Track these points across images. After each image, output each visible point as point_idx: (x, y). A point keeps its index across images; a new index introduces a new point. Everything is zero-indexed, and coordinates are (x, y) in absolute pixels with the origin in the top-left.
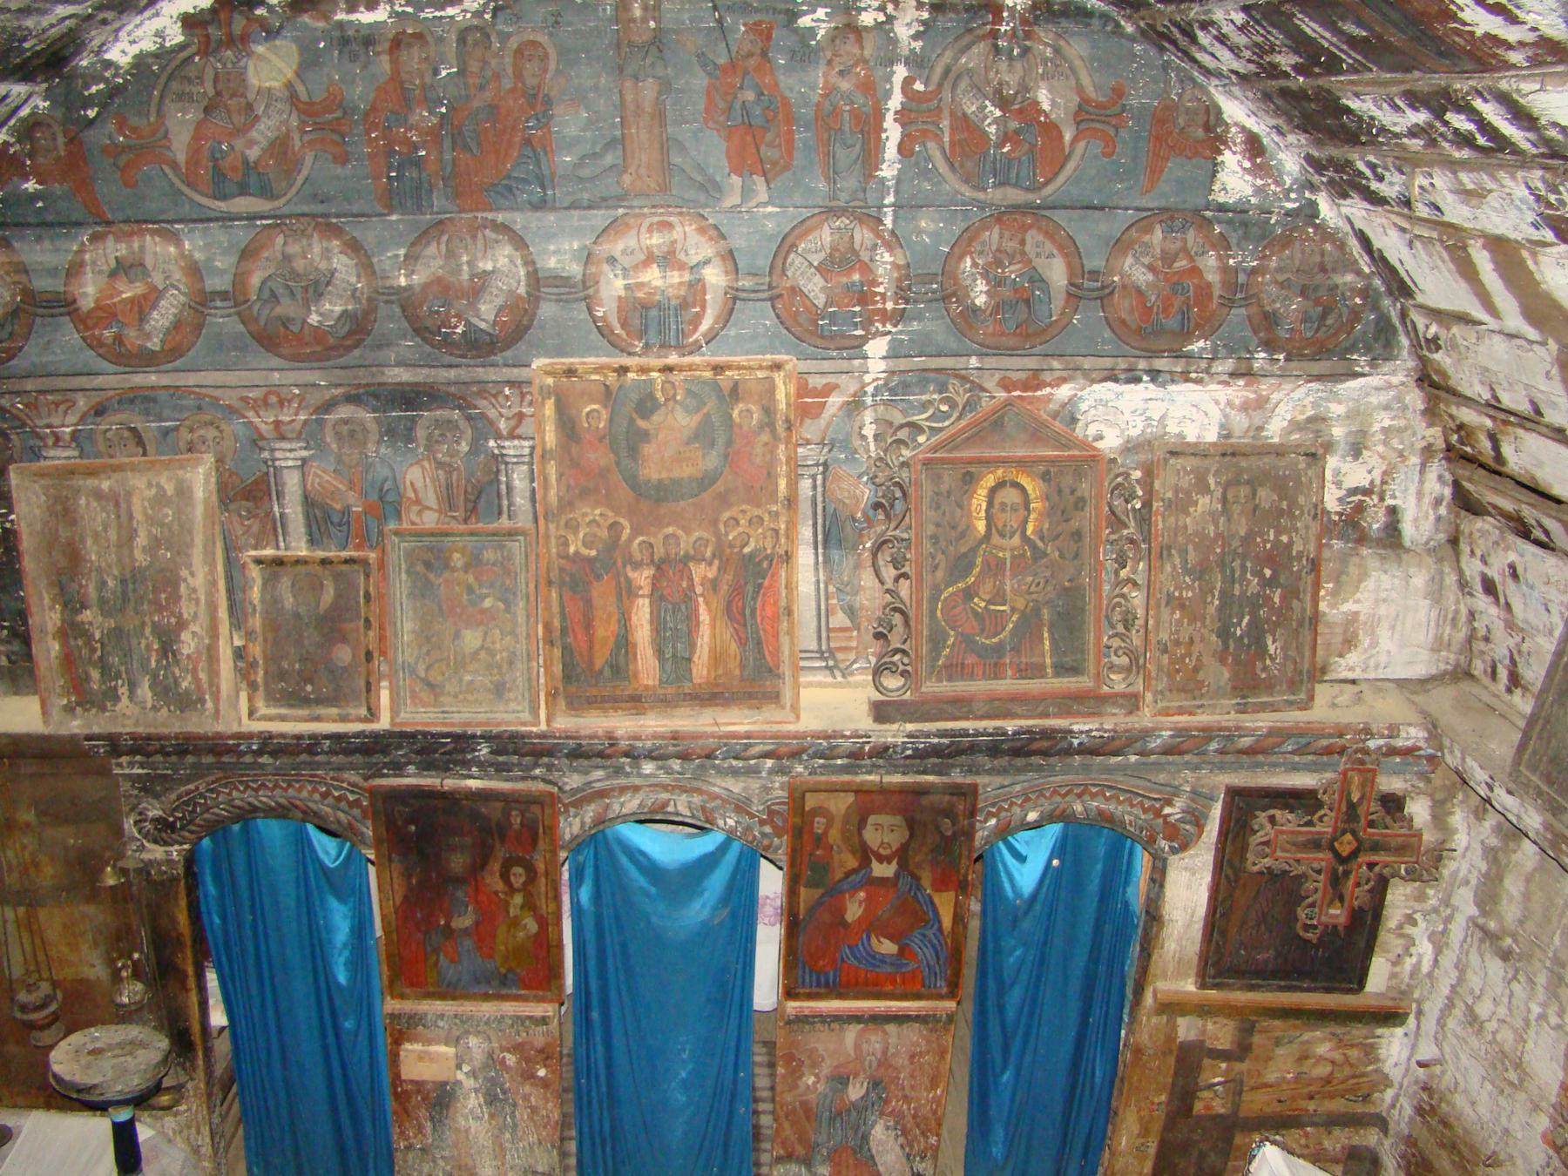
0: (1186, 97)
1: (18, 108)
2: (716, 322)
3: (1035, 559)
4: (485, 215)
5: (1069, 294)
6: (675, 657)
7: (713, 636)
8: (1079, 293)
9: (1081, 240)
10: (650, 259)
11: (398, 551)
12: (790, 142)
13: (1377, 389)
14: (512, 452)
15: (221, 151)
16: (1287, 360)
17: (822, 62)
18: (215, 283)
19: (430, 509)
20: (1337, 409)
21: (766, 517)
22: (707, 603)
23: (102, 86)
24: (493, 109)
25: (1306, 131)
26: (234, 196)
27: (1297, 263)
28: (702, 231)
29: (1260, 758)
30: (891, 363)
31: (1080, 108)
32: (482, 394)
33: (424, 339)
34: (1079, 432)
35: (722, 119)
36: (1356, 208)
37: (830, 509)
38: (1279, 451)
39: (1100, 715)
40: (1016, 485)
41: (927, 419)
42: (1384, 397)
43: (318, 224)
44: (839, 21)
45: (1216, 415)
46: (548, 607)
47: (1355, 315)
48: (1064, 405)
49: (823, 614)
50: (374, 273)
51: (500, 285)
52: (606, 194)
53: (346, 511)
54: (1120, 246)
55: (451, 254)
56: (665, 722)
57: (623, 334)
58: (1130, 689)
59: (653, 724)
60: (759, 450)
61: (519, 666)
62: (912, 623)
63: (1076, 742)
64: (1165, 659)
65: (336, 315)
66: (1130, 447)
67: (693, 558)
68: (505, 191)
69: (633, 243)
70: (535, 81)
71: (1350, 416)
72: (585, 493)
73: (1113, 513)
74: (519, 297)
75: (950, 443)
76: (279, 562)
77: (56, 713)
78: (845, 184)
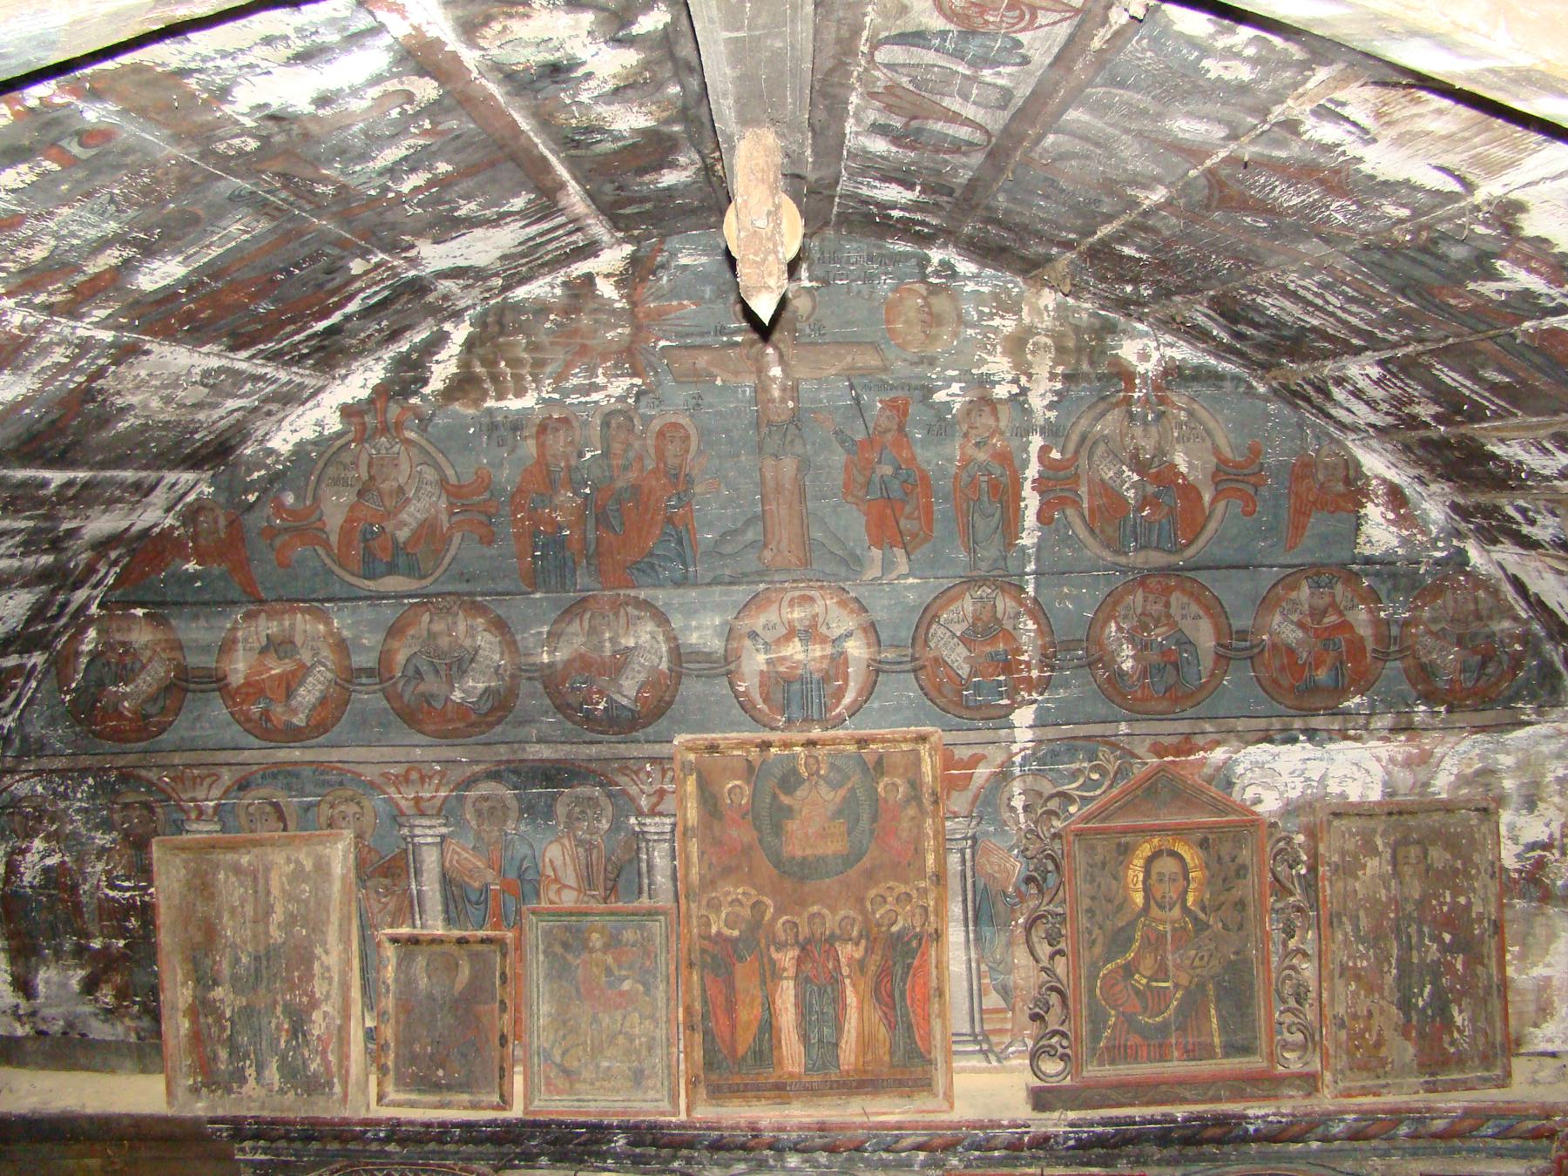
0: (1325, 451)
1: (185, 494)
2: (859, 694)
3: (1198, 932)
4: (628, 592)
6: (822, 1048)
7: (861, 1019)
10: (791, 633)
11: (535, 930)
12: (929, 512)
13: (1547, 737)
14: (653, 829)
15: (372, 532)
16: (1449, 711)
18: (360, 660)
20: (1506, 761)
21: (914, 894)
22: (854, 985)
25: (1449, 480)
26: (382, 576)
27: (1451, 612)
28: (842, 604)
29: (1457, 1142)
30: (1039, 731)
32: (624, 770)
33: (565, 715)
35: (861, 494)
36: (1507, 554)
37: (981, 883)
38: (1447, 808)
39: (1276, 1097)
40: (1173, 854)
41: (1077, 789)
42: (1554, 746)
45: (1378, 771)
46: (688, 991)
47: (1516, 662)
48: (1218, 769)
49: (975, 994)
50: (517, 650)
51: (643, 661)
52: (747, 570)
53: (485, 889)
54: (1266, 603)
55: (593, 631)
56: (812, 1111)
57: (765, 708)
58: (1307, 1069)
59: (799, 1114)
60: (905, 824)
61: (659, 1052)
62: (1071, 1003)
63: (1251, 1128)
64: (1343, 1035)
65: (479, 692)
66: (1291, 810)
67: (839, 938)
68: (645, 568)
69: (774, 618)
70: (677, 461)
71: (1521, 766)
72: (727, 872)
74: (662, 673)
75: (1103, 813)
76: (414, 941)
77: (181, 1093)
78: (986, 554)
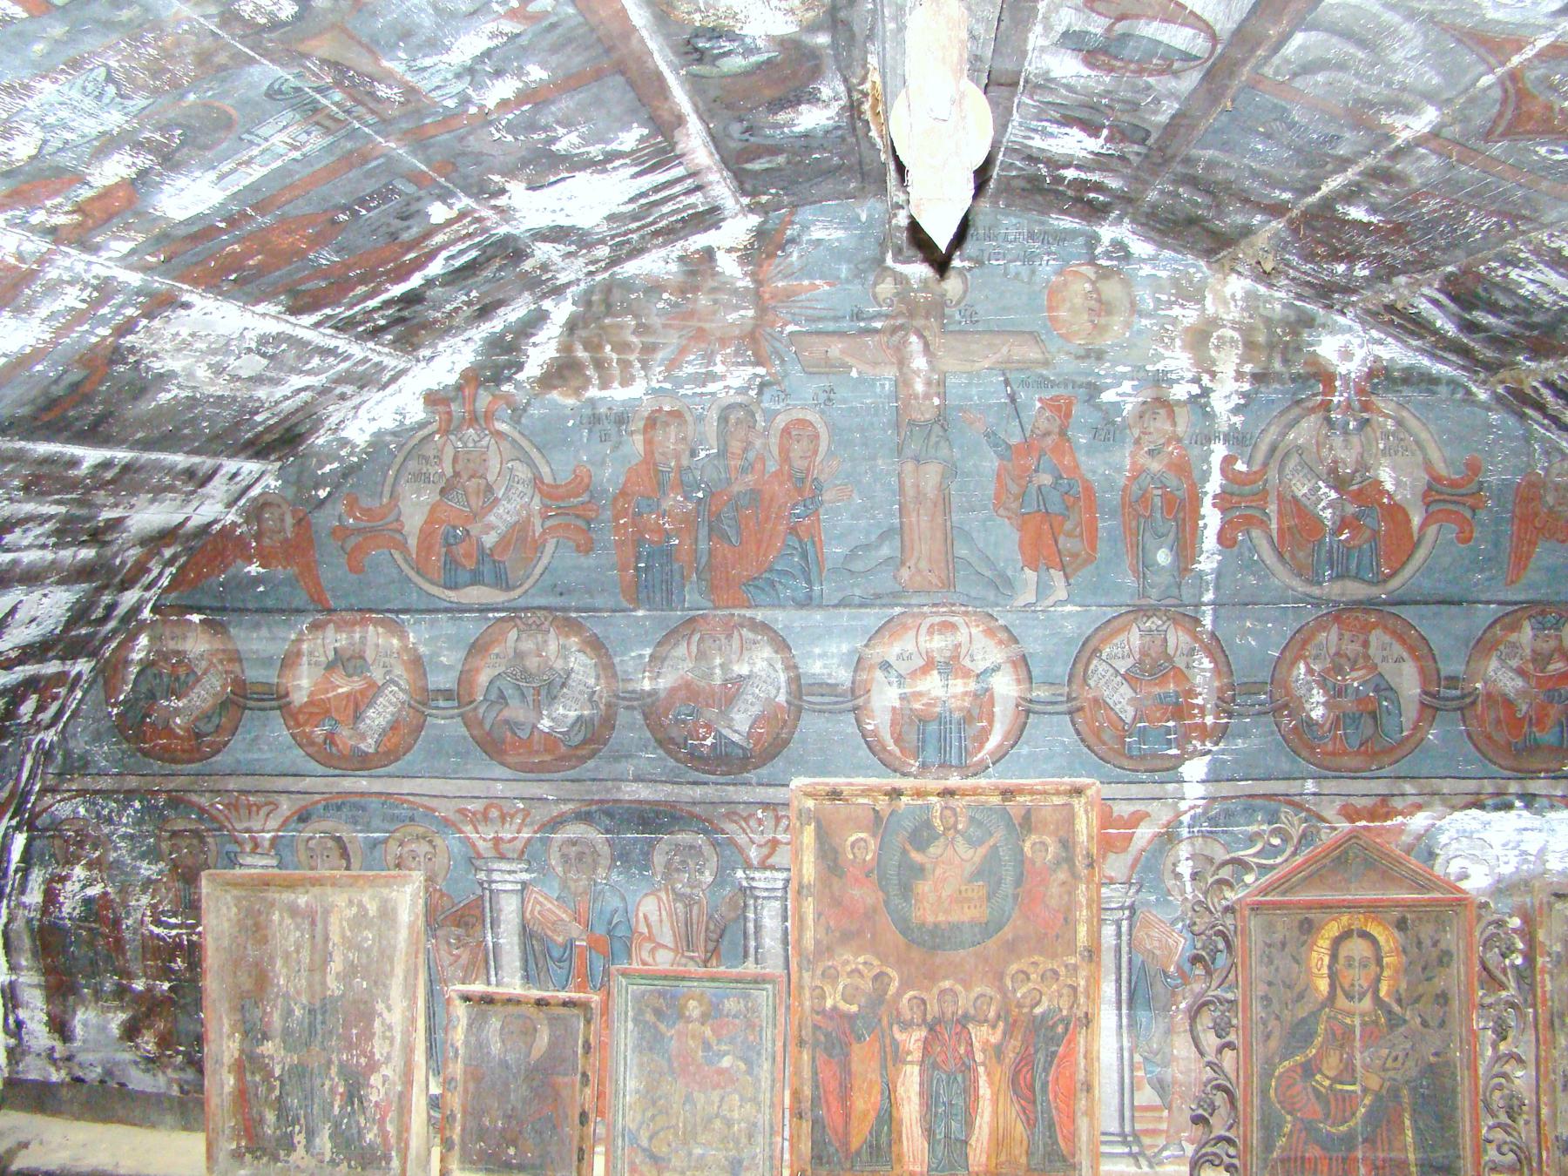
0: (1554, 471)
1: (249, 487)
2: (1006, 738)
5: (1422, 703)
7: (995, 1113)
8: (1435, 703)
9: (1436, 641)
10: (929, 665)
11: (625, 994)
14: (762, 885)
15: (455, 536)
17: (1129, 441)
18: (440, 680)
19: (665, 947)
21: (1062, 971)
23: (336, 465)
24: (755, 495)
28: (989, 632)
30: (1211, 788)
31: (1430, 488)
32: (729, 816)
34: (1438, 869)
35: (1014, 506)
37: (1138, 960)
40: (1364, 935)
41: (1255, 855)
43: (555, 618)
44: (1147, 395)
46: (797, 1072)
48: (1419, 837)
49: (1127, 1088)
50: (615, 675)
54: (1483, 646)
55: (701, 656)
57: (897, 751)
60: (1055, 890)
61: (760, 1139)
65: (570, 721)
66: (1503, 888)
67: (973, 1019)
68: (763, 585)
69: (910, 646)
70: (805, 463)
72: (846, 937)
73: (1485, 968)
74: (779, 706)
76: (488, 1000)
78: (1157, 579)
